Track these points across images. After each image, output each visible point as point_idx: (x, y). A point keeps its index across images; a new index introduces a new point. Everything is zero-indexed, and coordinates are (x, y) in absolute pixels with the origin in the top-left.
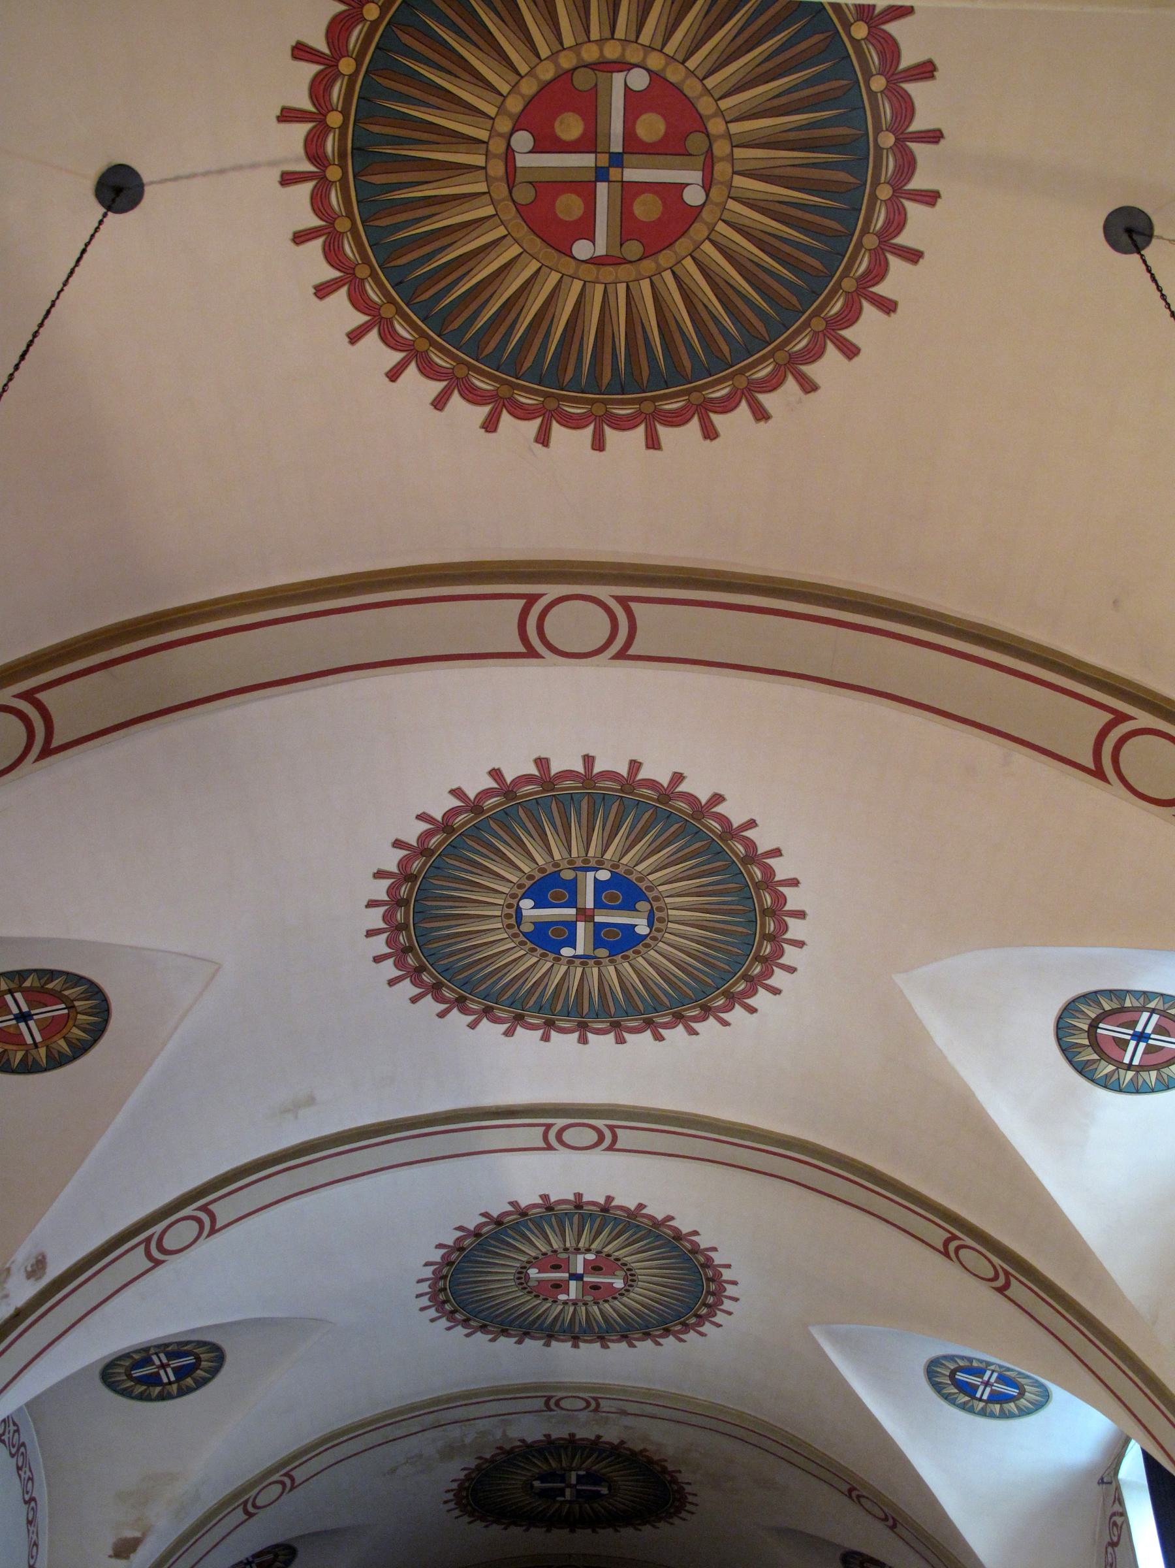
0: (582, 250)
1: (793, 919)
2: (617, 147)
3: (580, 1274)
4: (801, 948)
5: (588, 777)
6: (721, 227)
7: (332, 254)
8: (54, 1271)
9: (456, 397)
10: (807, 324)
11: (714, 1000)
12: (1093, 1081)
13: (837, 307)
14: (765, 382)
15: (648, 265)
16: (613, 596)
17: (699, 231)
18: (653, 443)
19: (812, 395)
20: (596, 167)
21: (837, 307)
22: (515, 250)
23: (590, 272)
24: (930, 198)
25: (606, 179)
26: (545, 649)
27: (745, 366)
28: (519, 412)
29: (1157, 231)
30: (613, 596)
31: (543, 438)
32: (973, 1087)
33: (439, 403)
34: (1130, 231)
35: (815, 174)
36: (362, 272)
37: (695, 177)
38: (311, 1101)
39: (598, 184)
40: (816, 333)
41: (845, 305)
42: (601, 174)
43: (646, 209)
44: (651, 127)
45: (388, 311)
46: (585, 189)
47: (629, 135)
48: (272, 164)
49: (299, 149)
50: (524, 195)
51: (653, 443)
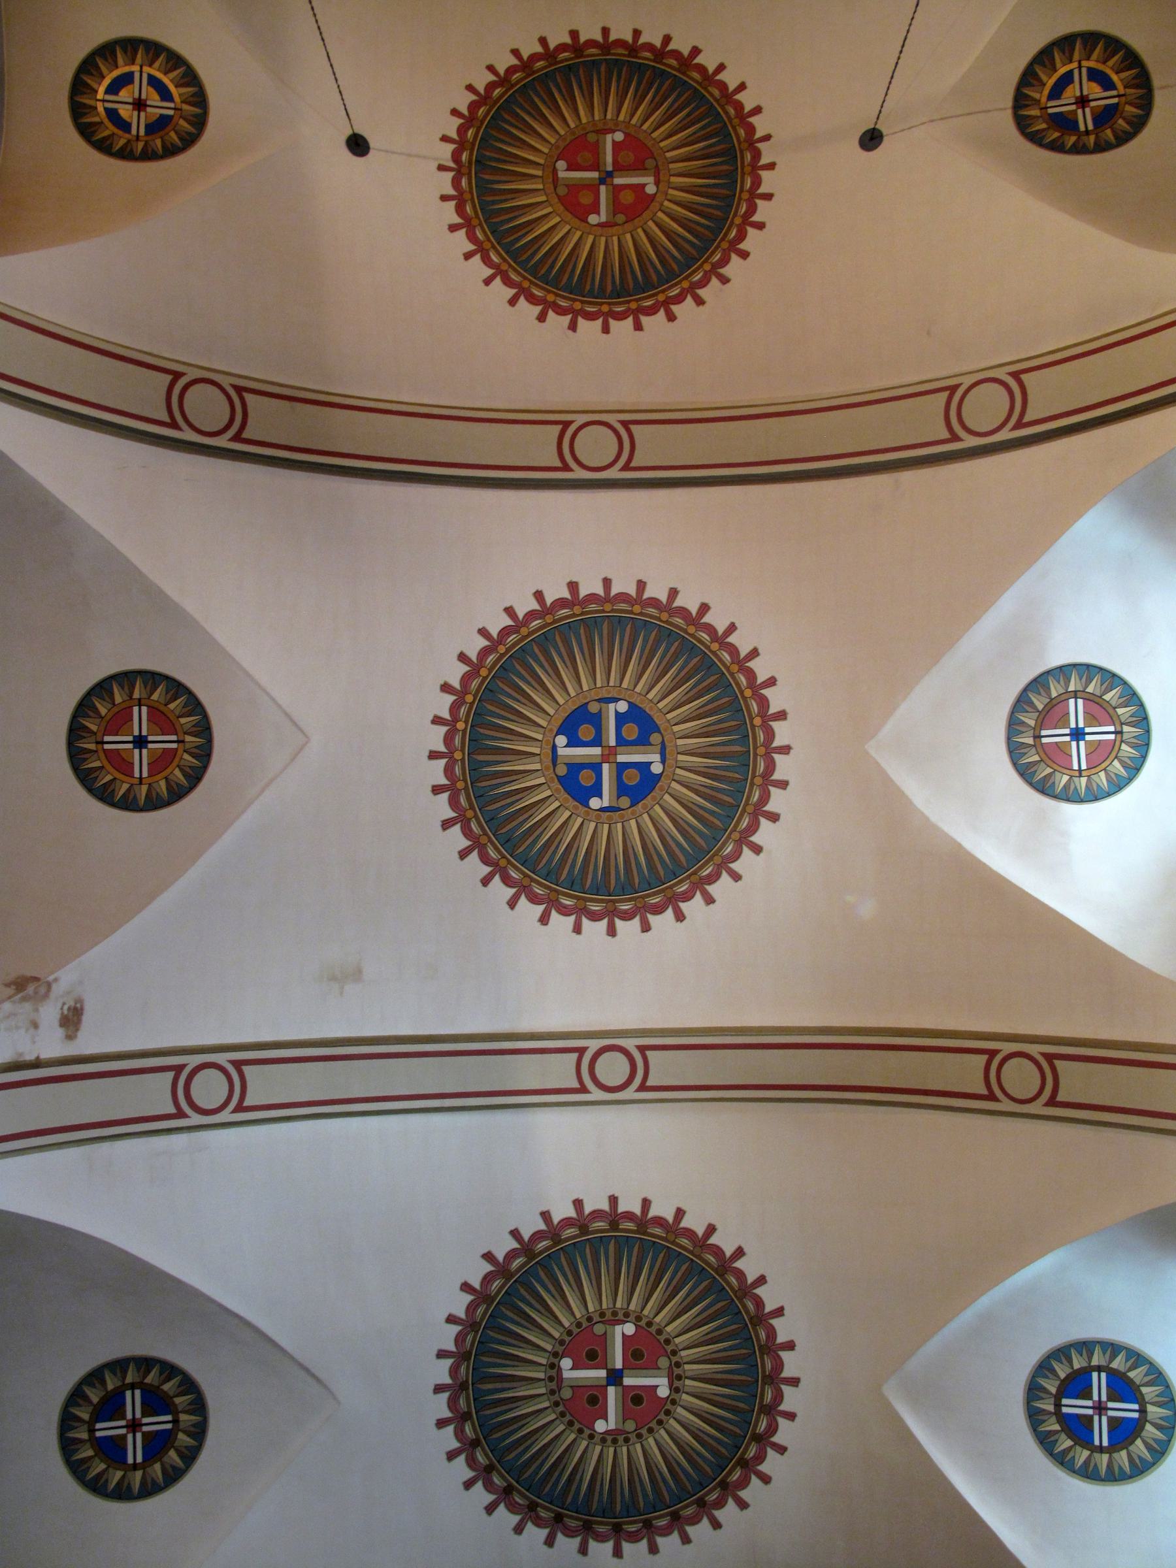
0: (595, 803)
1: (777, 723)
2: (610, 168)
3: (619, 1370)
4: (788, 753)
5: (606, 45)
6: (666, 203)
7: (460, 209)
8: (88, 1042)
9: (522, 300)
10: (756, 755)
11: (757, 1426)
12: (1055, 797)
13: (733, 233)
14: (700, 282)
15: (629, 226)
16: (619, 421)
17: (655, 206)
18: (638, 327)
19: (728, 285)
20: (602, 755)
21: (733, 233)
22: (557, 219)
23: (599, 230)
24: (771, 166)
25: (607, 172)
26: (575, 464)
27: (717, 850)
28: (560, 311)
29: (884, 133)
30: (619, 421)
31: (573, 327)
32: (959, 840)
33: (513, 302)
34: (872, 139)
35: (711, 169)
36: (475, 222)
37: (650, 180)
38: (357, 974)
39: (609, 1387)
40: (724, 250)
41: (738, 231)
42: (602, 181)
43: (628, 198)
44: (628, 157)
45: (487, 245)
46: (593, 188)
47: (615, 162)
48: (436, 159)
49: (449, 155)
50: (562, 191)
51: (638, 327)
